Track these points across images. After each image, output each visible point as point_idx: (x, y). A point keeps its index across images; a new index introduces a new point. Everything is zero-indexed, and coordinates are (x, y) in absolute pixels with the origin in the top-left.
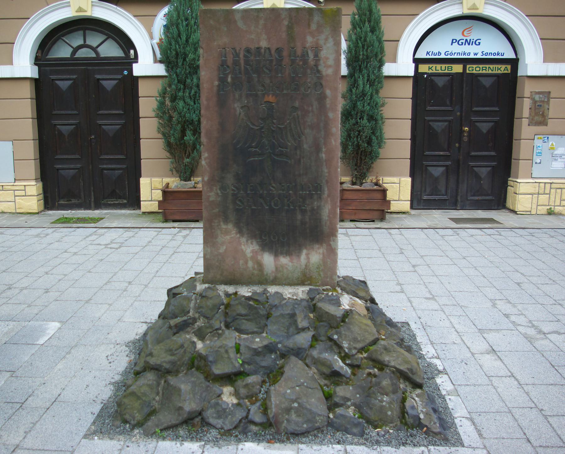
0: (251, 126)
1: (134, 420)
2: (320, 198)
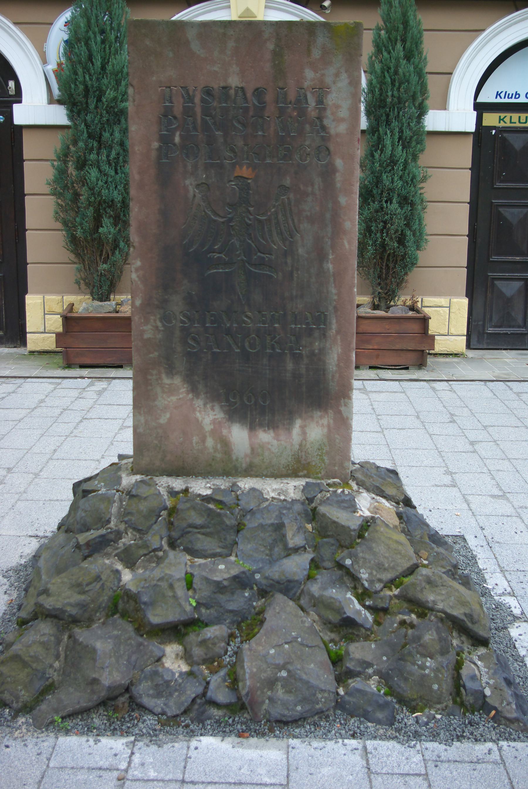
1: (17, 702)
2: (324, 335)
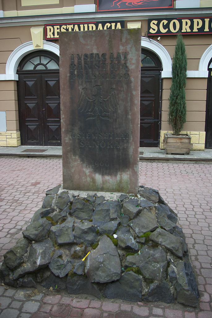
0: (88, 100)
2: (128, 142)
